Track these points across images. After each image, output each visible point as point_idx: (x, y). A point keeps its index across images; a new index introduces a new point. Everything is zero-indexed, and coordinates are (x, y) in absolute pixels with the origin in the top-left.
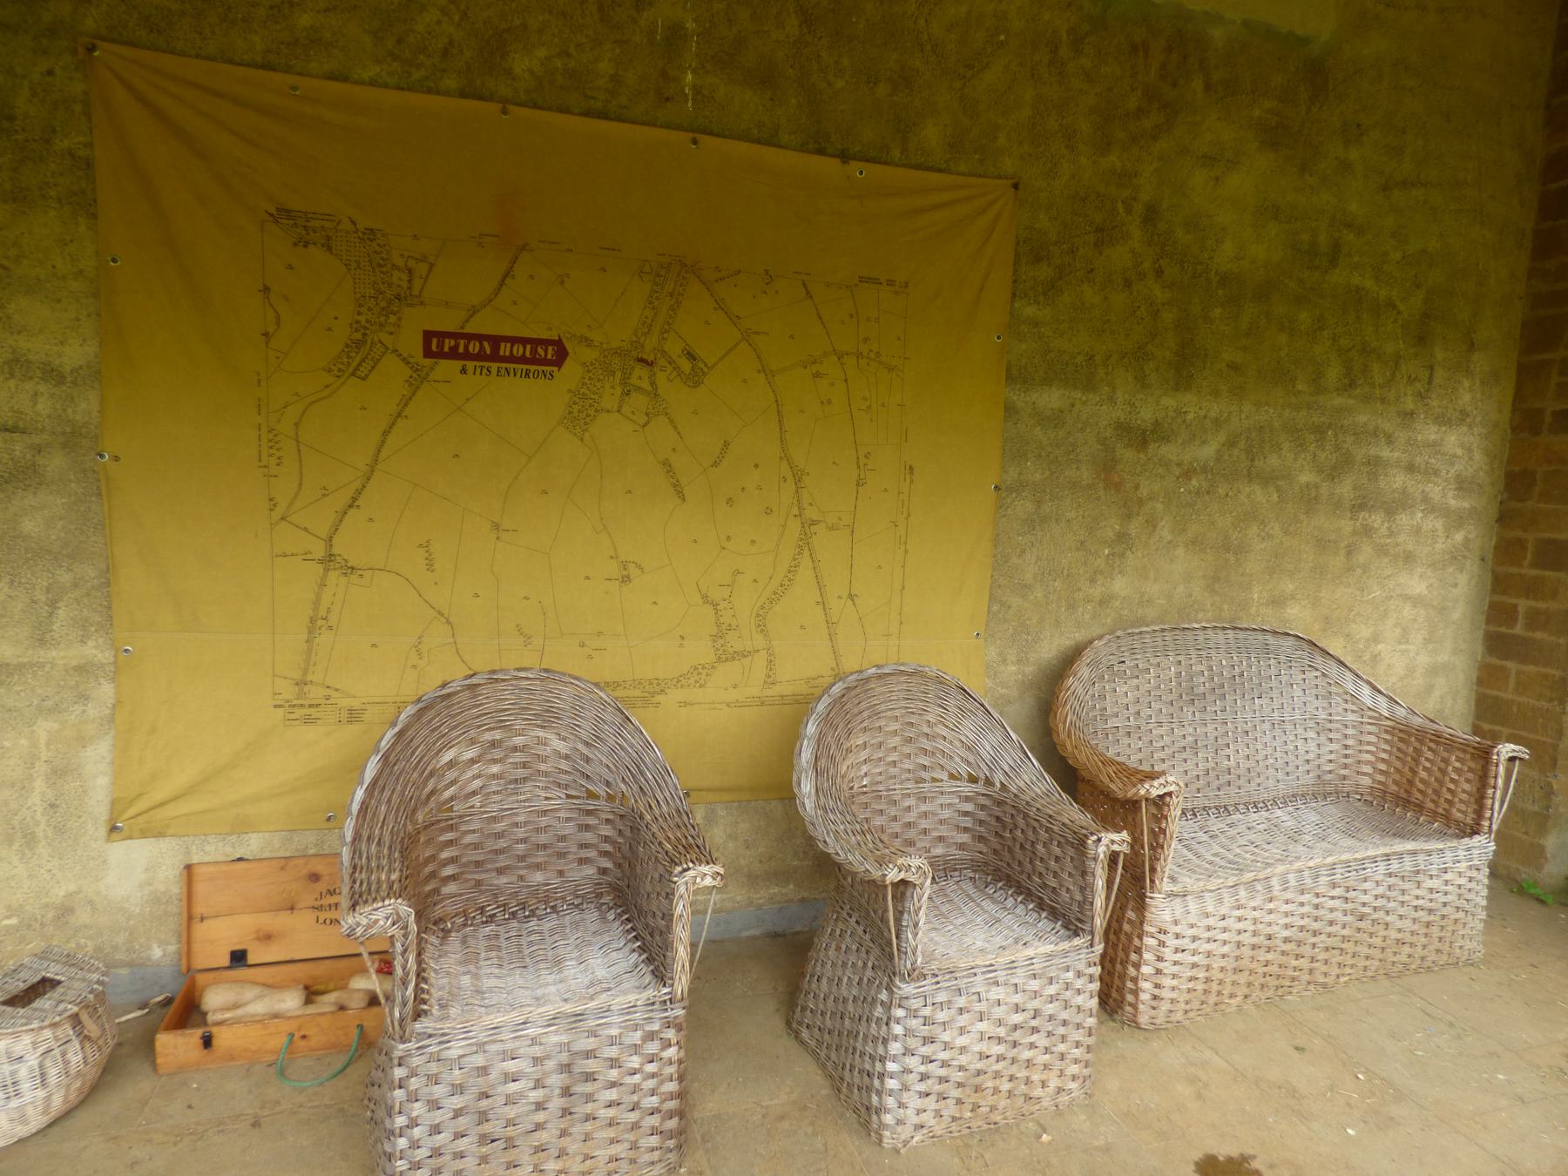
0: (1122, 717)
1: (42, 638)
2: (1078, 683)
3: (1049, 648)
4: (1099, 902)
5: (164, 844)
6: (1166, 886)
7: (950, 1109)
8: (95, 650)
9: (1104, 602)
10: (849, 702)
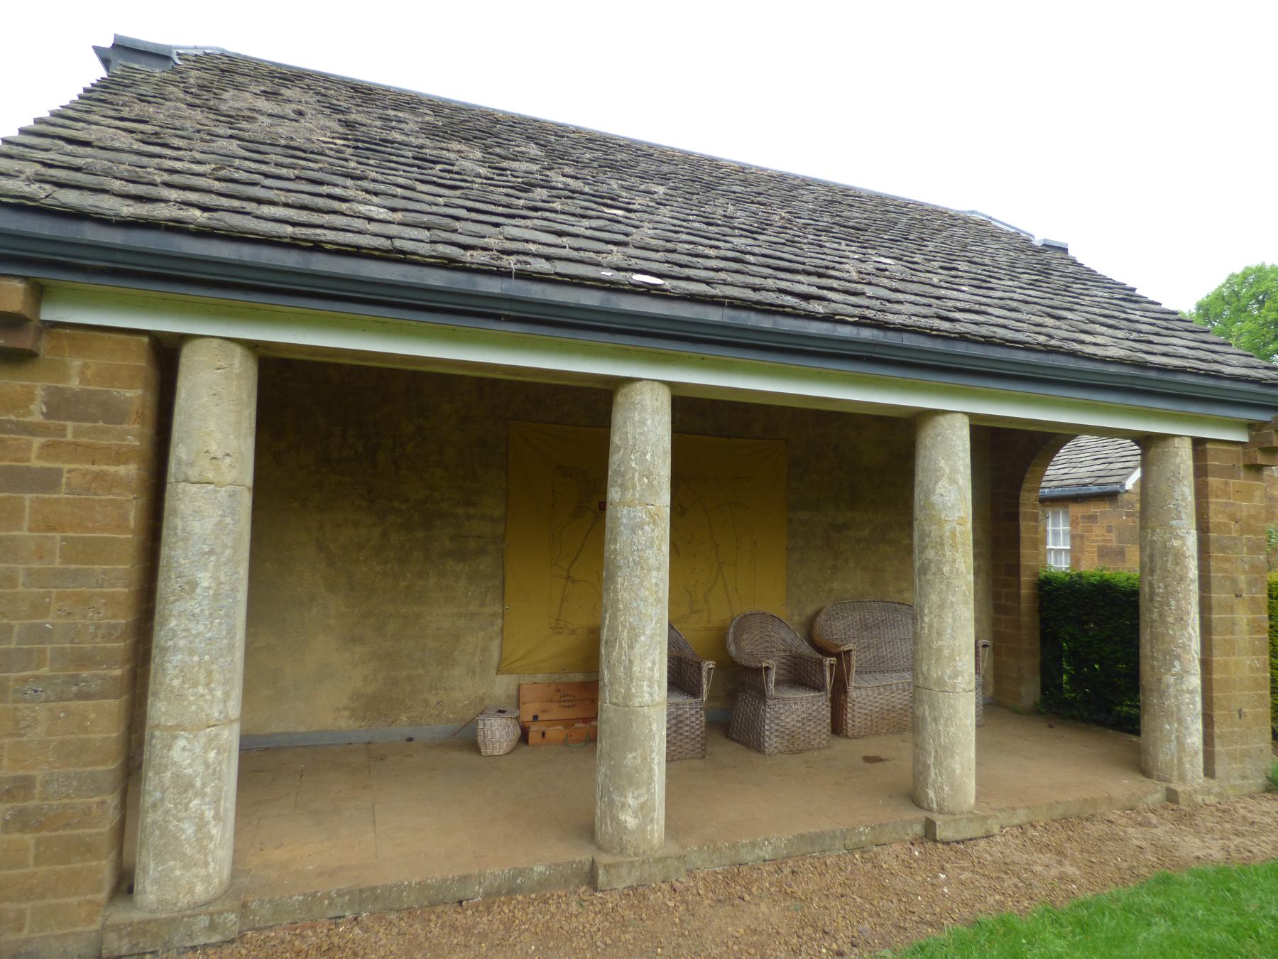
0: (838, 629)
1: (483, 604)
2: (822, 619)
3: (809, 610)
4: (828, 680)
5: (513, 677)
6: (853, 684)
7: (786, 743)
8: (497, 609)
9: (831, 591)
10: (742, 624)
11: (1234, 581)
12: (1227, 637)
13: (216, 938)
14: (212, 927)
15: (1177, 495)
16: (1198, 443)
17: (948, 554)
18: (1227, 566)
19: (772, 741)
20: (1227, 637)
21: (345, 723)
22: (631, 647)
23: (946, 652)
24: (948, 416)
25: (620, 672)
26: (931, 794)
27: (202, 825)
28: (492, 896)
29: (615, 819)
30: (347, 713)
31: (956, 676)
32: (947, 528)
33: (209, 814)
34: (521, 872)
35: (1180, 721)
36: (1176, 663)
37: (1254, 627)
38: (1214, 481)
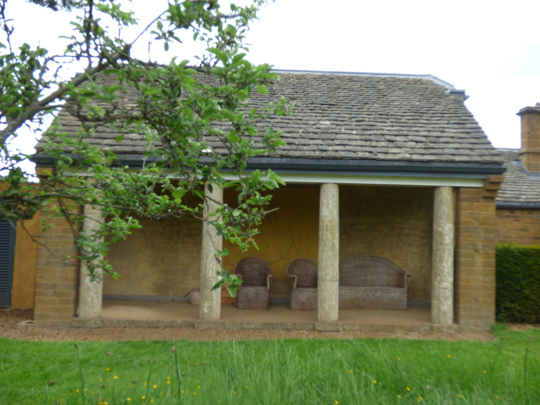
11: (474, 245)
12: (470, 268)
13: (96, 326)
14: (95, 323)
15: (441, 210)
16: (456, 190)
17: (325, 233)
18: (470, 239)
19: (294, 305)
20: (470, 268)
21: (151, 293)
22: (206, 260)
23: (324, 267)
24: (327, 185)
25: (204, 267)
26: (319, 316)
27: (93, 299)
28: (166, 327)
29: (202, 310)
30: (151, 290)
31: (326, 275)
32: (325, 224)
33: (94, 297)
34: (174, 322)
35: (439, 300)
36: (439, 277)
37: (486, 265)
38: (463, 204)
